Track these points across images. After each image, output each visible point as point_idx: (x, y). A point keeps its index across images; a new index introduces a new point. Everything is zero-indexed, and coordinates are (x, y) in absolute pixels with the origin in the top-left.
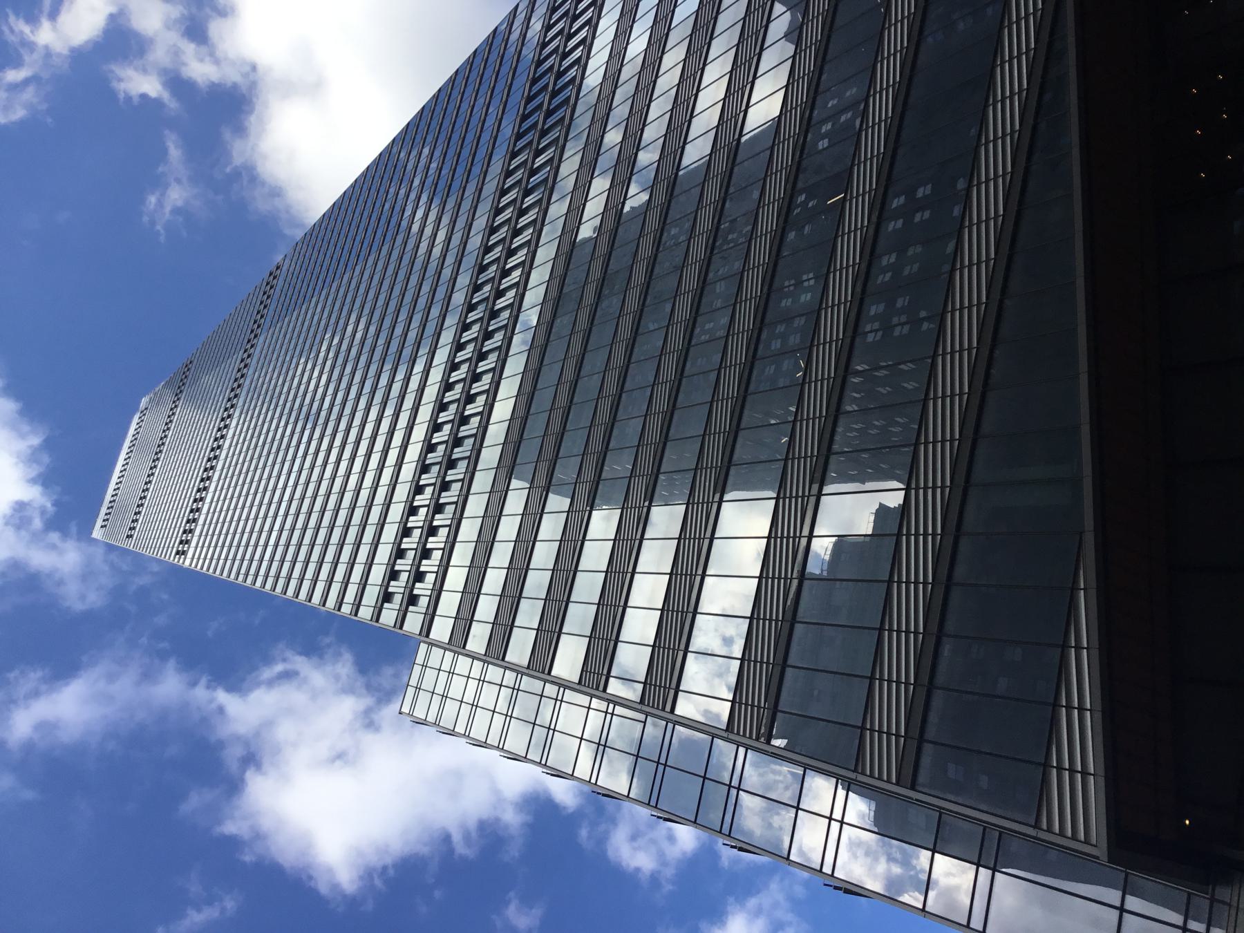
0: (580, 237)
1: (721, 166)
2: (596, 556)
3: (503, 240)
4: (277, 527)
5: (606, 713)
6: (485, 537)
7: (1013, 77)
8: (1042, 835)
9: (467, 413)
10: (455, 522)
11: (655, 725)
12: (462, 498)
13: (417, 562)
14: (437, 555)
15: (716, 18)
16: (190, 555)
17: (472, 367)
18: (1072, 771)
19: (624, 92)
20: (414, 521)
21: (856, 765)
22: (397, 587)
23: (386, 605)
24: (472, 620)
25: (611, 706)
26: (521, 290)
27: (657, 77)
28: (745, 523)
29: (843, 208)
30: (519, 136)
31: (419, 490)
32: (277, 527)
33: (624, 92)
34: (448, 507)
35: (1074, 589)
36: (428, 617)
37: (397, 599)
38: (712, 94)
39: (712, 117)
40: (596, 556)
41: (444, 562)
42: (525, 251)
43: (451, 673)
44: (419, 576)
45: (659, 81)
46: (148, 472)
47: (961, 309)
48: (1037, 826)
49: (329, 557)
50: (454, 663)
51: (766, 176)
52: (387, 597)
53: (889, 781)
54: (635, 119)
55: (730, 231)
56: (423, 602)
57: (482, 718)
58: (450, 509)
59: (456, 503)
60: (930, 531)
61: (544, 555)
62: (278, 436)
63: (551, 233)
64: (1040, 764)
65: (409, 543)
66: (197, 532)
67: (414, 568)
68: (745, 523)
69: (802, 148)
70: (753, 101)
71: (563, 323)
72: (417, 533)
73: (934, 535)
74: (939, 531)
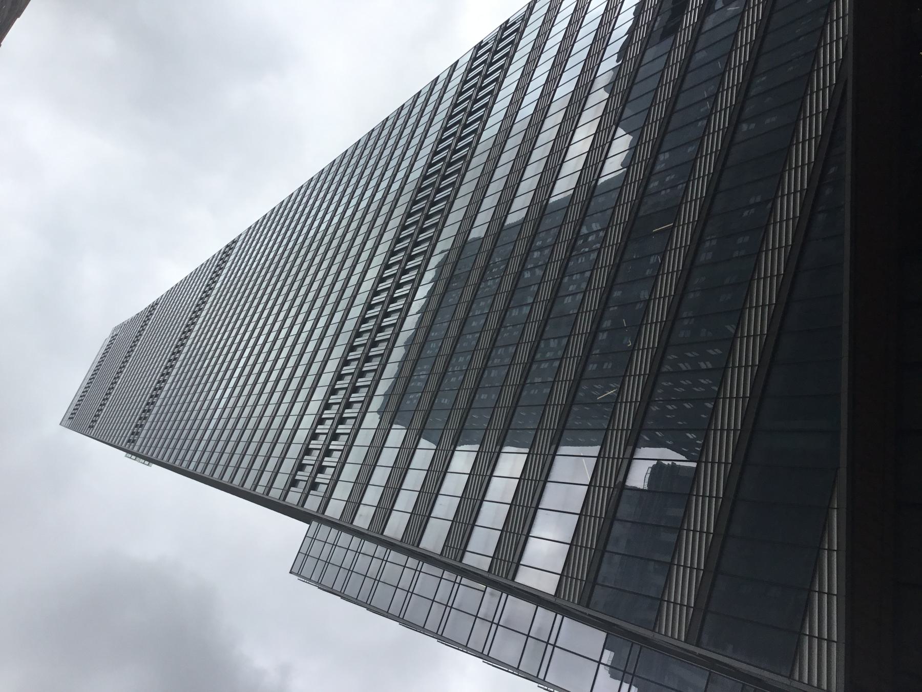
0: (471, 237)
1: (582, 196)
2: (454, 484)
3: (388, 289)
4: (201, 448)
5: (455, 582)
6: (361, 480)
7: (804, 153)
8: (796, 684)
9: (358, 384)
10: (340, 465)
11: (492, 594)
12: (354, 431)
13: (327, 442)
14: (330, 471)
15: (581, 114)
16: (138, 443)
17: (360, 366)
18: (820, 638)
19: (514, 142)
20: (308, 460)
21: (654, 627)
22: (302, 476)
23: (292, 489)
24: (360, 503)
25: (459, 578)
26: (397, 330)
27: (539, 133)
28: (574, 468)
29: (672, 232)
30: (431, 165)
31: (321, 421)
32: (196, 459)
33: (514, 142)
34: (342, 436)
35: (829, 508)
36: (325, 500)
37: (302, 485)
38: (581, 144)
39: (579, 164)
40: (454, 484)
41: (328, 495)
42: (415, 272)
43: (334, 545)
44: (321, 469)
45: (541, 136)
46: (101, 401)
47: (781, 222)
48: (791, 677)
49: (245, 463)
50: (337, 538)
51: (623, 185)
52: (294, 483)
53: (679, 639)
54: (514, 177)
55: (583, 246)
56: (322, 488)
57: (355, 580)
58: (337, 455)
59: (349, 434)
60: (723, 460)
61: (414, 479)
62: (202, 398)
63: (449, 232)
64: (658, 599)
65: (309, 460)
66: (142, 435)
67: (311, 479)
68: (574, 468)
69: (643, 192)
70: (610, 154)
71: (445, 315)
72: (309, 469)
73: (726, 463)
74: (730, 461)
